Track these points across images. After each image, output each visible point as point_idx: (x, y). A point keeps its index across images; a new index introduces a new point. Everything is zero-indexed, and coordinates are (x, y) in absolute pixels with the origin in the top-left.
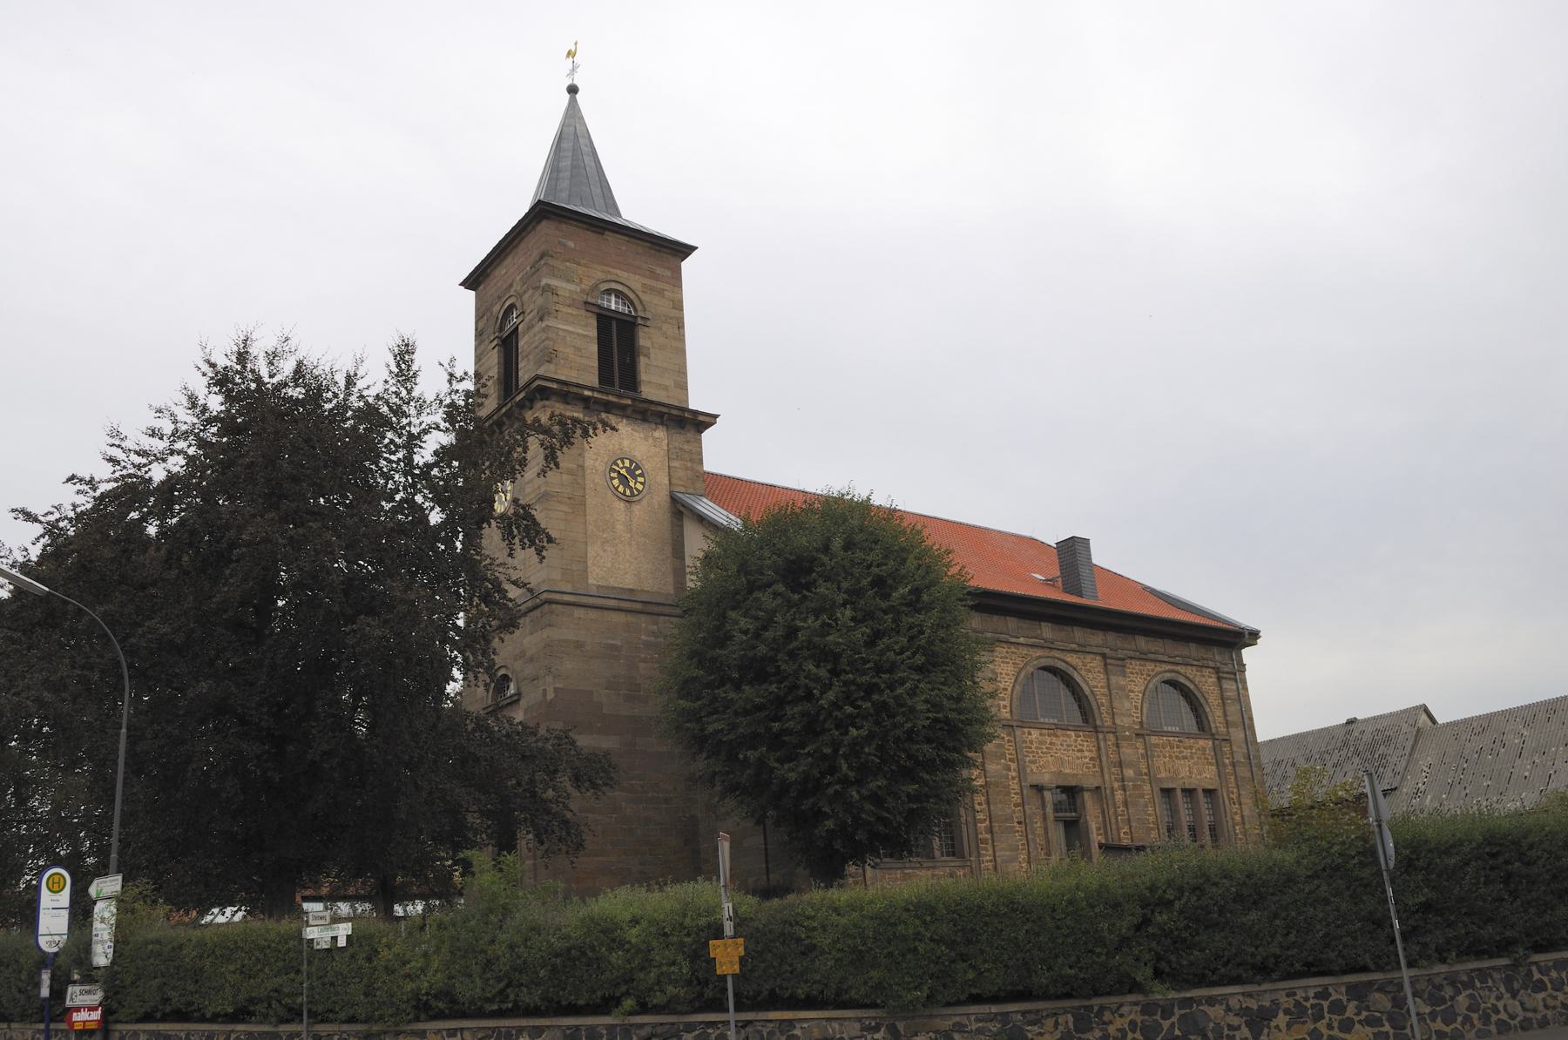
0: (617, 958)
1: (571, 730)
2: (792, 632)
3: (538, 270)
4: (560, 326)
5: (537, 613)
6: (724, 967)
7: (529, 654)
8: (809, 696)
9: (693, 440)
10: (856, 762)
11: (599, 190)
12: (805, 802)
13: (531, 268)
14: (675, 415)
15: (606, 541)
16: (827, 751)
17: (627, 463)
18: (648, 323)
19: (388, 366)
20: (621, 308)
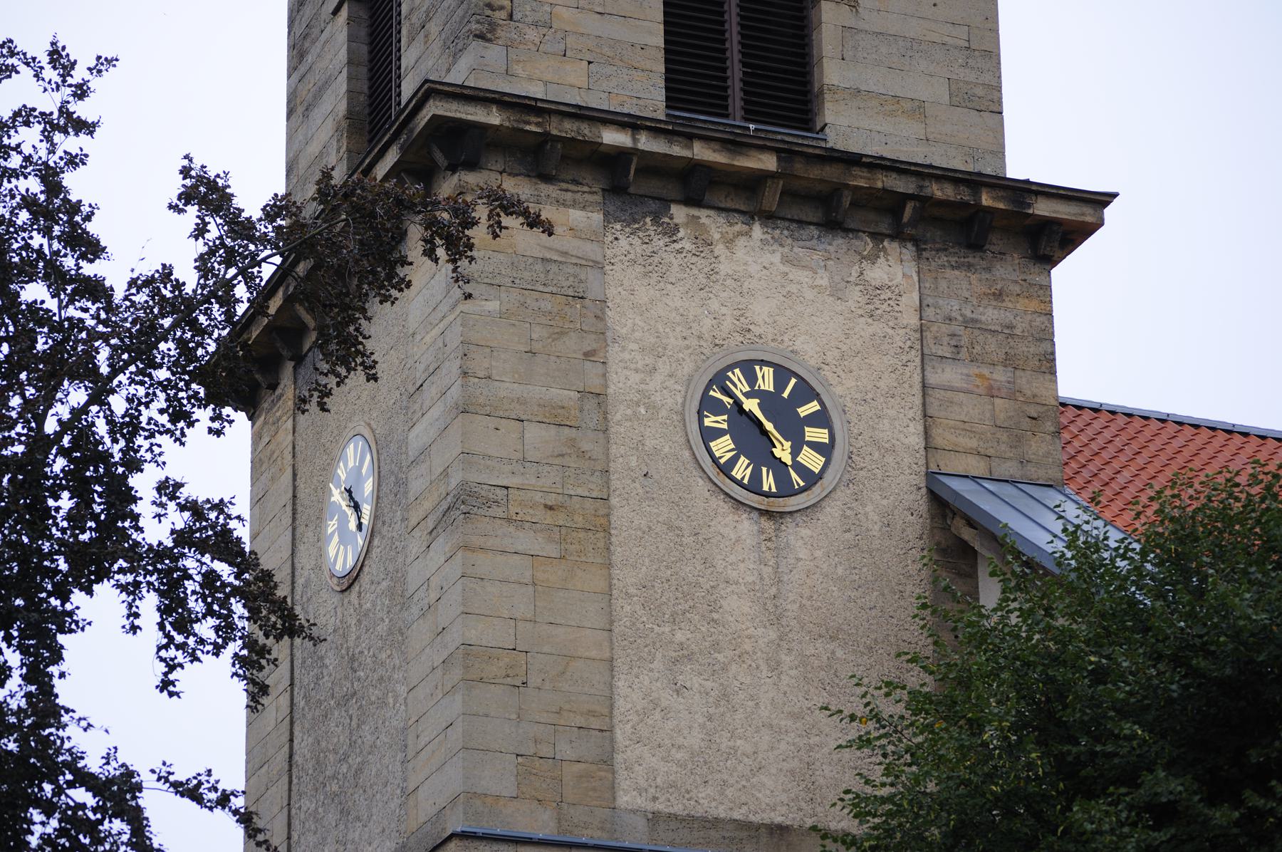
15: (684, 656)
17: (766, 380)
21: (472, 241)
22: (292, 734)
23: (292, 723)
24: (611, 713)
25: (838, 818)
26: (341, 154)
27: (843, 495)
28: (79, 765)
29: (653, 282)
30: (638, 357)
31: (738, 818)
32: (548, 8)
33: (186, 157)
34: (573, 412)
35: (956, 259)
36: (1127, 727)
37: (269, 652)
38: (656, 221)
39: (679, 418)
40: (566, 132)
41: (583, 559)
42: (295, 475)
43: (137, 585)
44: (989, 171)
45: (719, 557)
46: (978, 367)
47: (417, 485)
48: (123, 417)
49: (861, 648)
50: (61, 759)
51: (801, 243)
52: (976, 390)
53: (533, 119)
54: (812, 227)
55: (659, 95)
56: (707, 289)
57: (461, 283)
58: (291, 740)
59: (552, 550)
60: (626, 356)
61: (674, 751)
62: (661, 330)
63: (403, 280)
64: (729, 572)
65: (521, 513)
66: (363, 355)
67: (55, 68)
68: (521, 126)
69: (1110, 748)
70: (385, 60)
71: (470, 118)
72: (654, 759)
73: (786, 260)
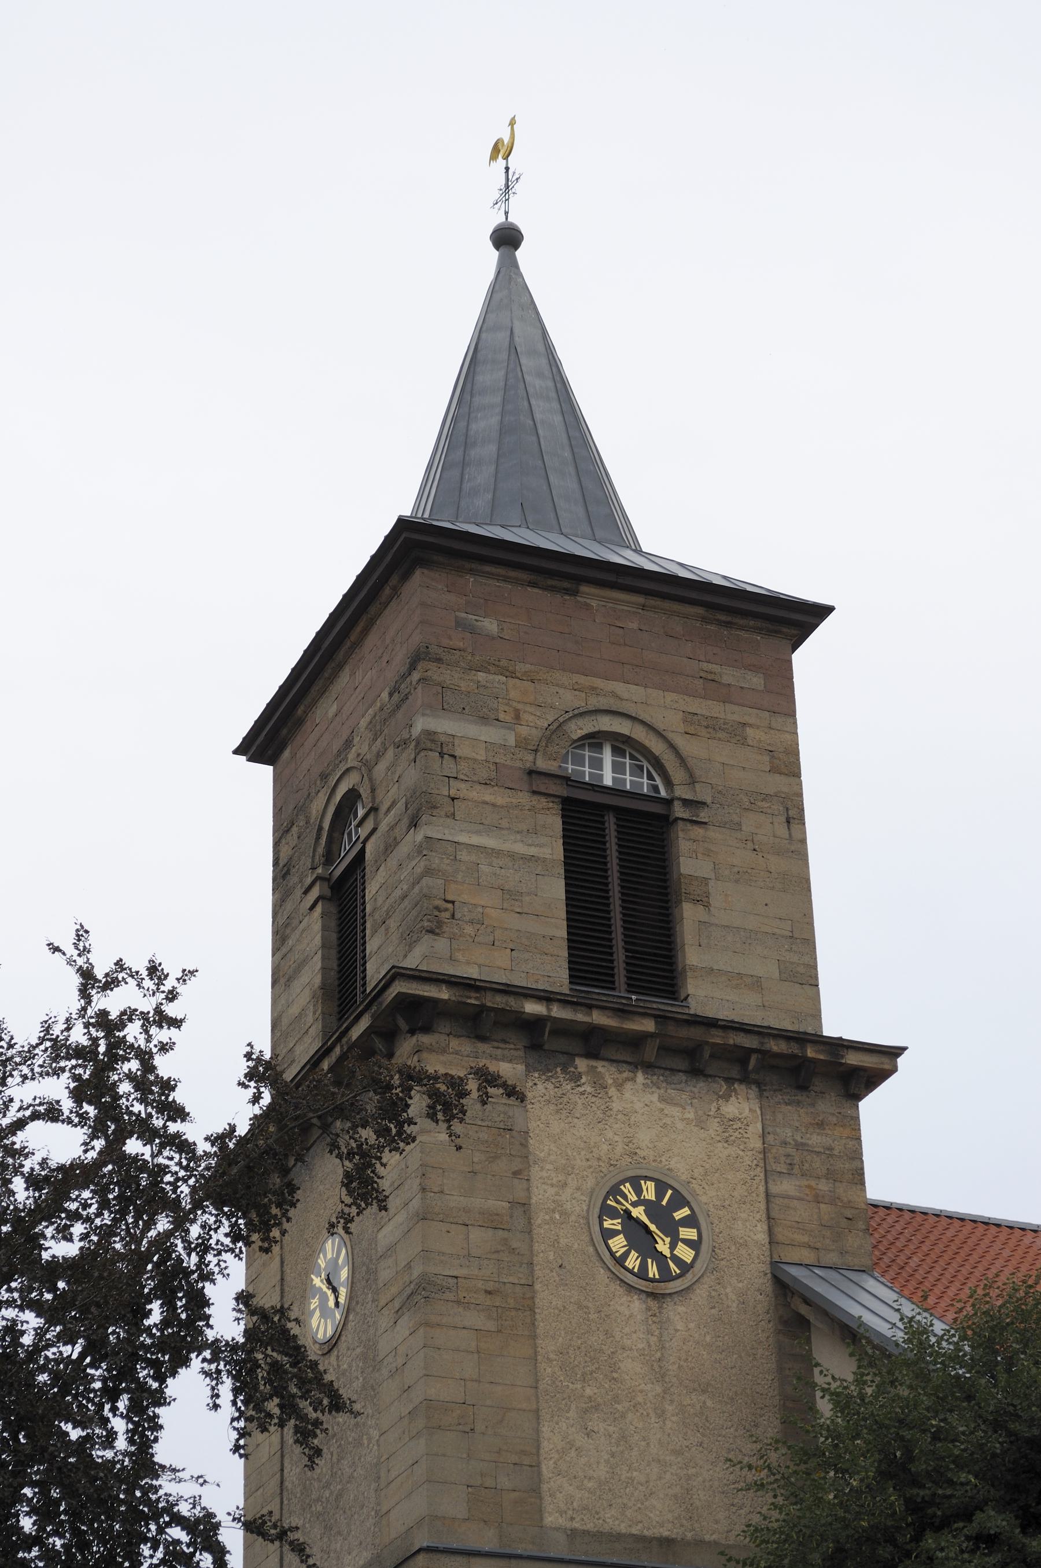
17: (649, 1191)
20: (629, 781)
21: (465, 1108)
22: (282, 1465)
23: (282, 1456)
24: (538, 1452)
25: (710, 1532)
26: (317, 1016)
27: (709, 1280)
28: (175, 1510)
29: (563, 1117)
30: (553, 1175)
31: (635, 1533)
32: (480, 910)
33: (249, 1044)
34: (505, 1218)
35: (789, 1097)
36: (963, 1477)
37: (322, 1423)
38: (564, 1070)
39: (585, 1221)
40: (498, 1004)
41: (515, 1332)
43: (218, 1372)
44: (810, 1030)
45: (617, 1329)
46: (807, 1180)
47: (385, 1274)
48: (197, 1239)
49: (725, 1399)
50: (160, 1506)
51: (673, 1086)
52: (805, 1197)
53: (473, 994)
54: (681, 1074)
55: (565, 974)
56: (604, 1122)
57: (454, 1138)
58: (282, 1470)
59: (491, 1326)
60: (544, 1174)
61: (586, 1482)
62: (570, 1154)
63: (410, 1136)
64: (625, 1341)
65: (468, 1297)
66: (377, 1191)
67: (151, 979)
68: (464, 1000)
69: (949, 1492)
70: (352, 944)
71: (426, 994)
72: (571, 1488)
73: (661, 1099)
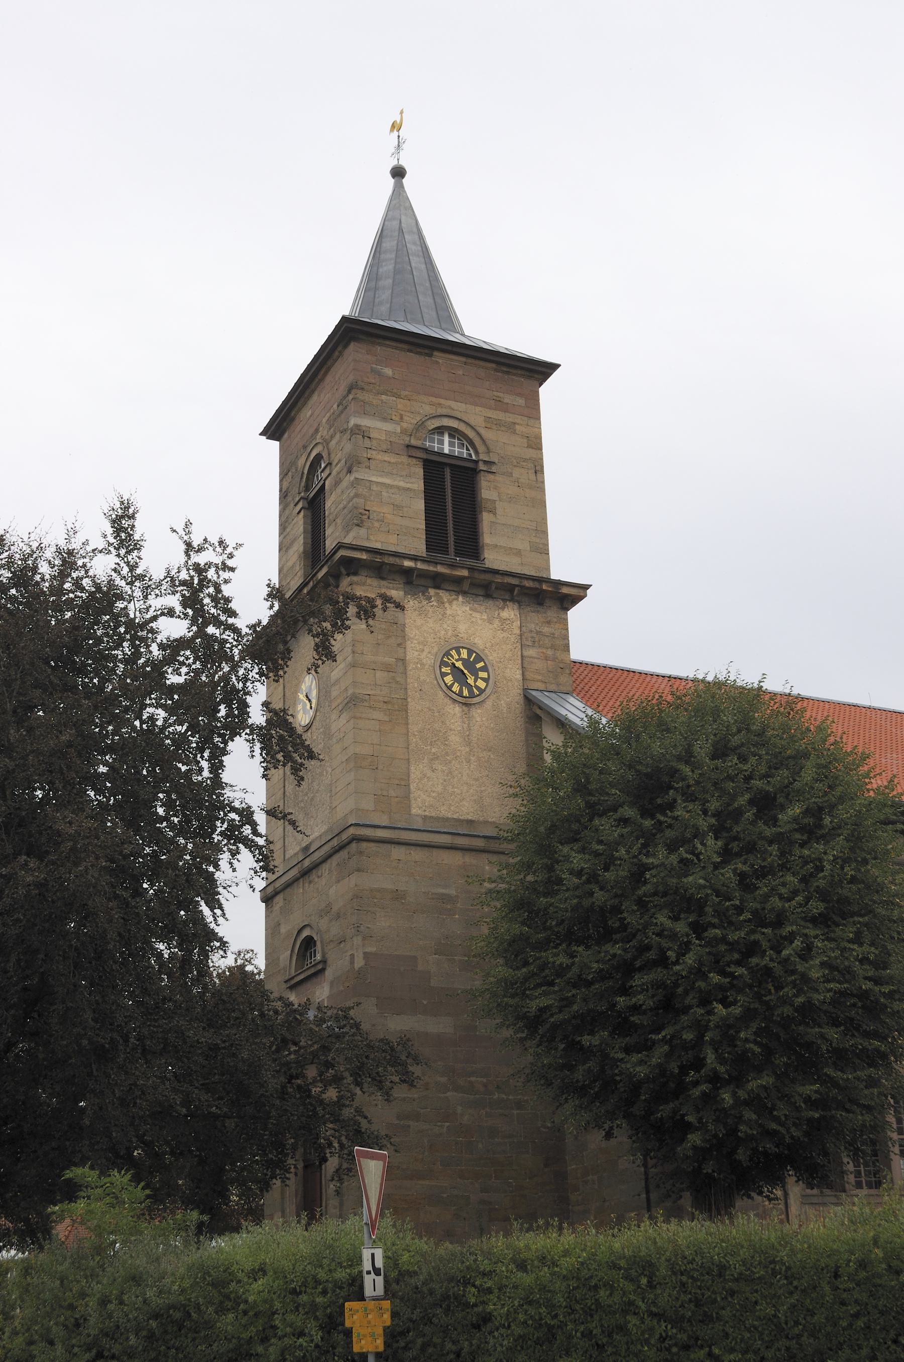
0: (228, 1322)
1: (353, 1008)
2: (638, 875)
3: (346, 407)
4: (374, 479)
5: (343, 854)
6: (363, 1342)
7: (335, 909)
8: (663, 961)
9: (555, 620)
10: (729, 1053)
11: (430, 300)
12: (661, 1108)
13: (338, 406)
14: (528, 588)
15: (435, 758)
16: (688, 1036)
17: (464, 654)
18: (494, 469)
19: (105, 536)
20: (457, 451)
23: (284, 780)
27: (493, 697)
36: (613, 791)
38: (423, 595)
42: (284, 687)
43: (253, 740)
44: (544, 576)
47: (335, 693)
53: (378, 557)
59: (387, 718)
60: (413, 645)
73: (471, 609)
